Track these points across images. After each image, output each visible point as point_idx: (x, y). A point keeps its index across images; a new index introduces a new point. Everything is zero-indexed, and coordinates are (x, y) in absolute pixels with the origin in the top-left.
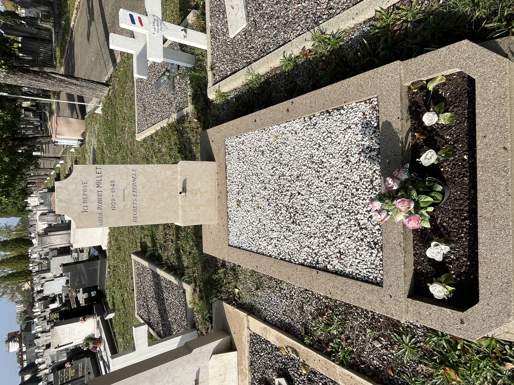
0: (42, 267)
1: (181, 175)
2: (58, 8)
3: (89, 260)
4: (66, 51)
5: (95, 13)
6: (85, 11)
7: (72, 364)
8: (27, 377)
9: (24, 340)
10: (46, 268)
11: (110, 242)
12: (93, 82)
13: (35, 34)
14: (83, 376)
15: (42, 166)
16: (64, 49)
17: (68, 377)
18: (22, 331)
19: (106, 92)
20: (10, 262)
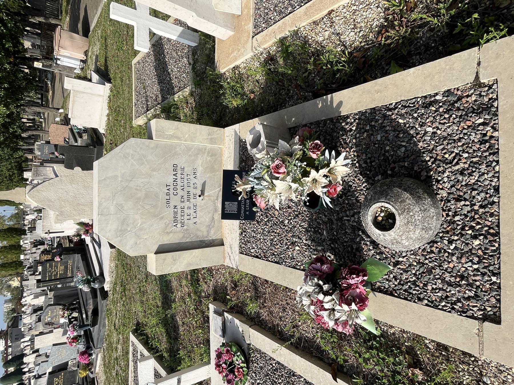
7: (61, 259)
8: (11, 369)
9: (11, 337)
17: (57, 273)
18: (8, 327)
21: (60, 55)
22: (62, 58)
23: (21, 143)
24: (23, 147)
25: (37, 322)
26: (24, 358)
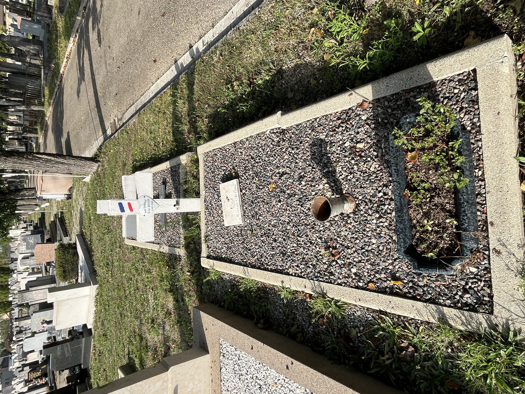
0: (22, 313)
1: (172, 383)
2: (48, 50)
3: (72, 339)
4: (55, 93)
5: (86, 74)
6: (75, 65)
10: (27, 315)
11: (96, 321)
13: (23, 70)
16: (54, 91)
19: (95, 168)
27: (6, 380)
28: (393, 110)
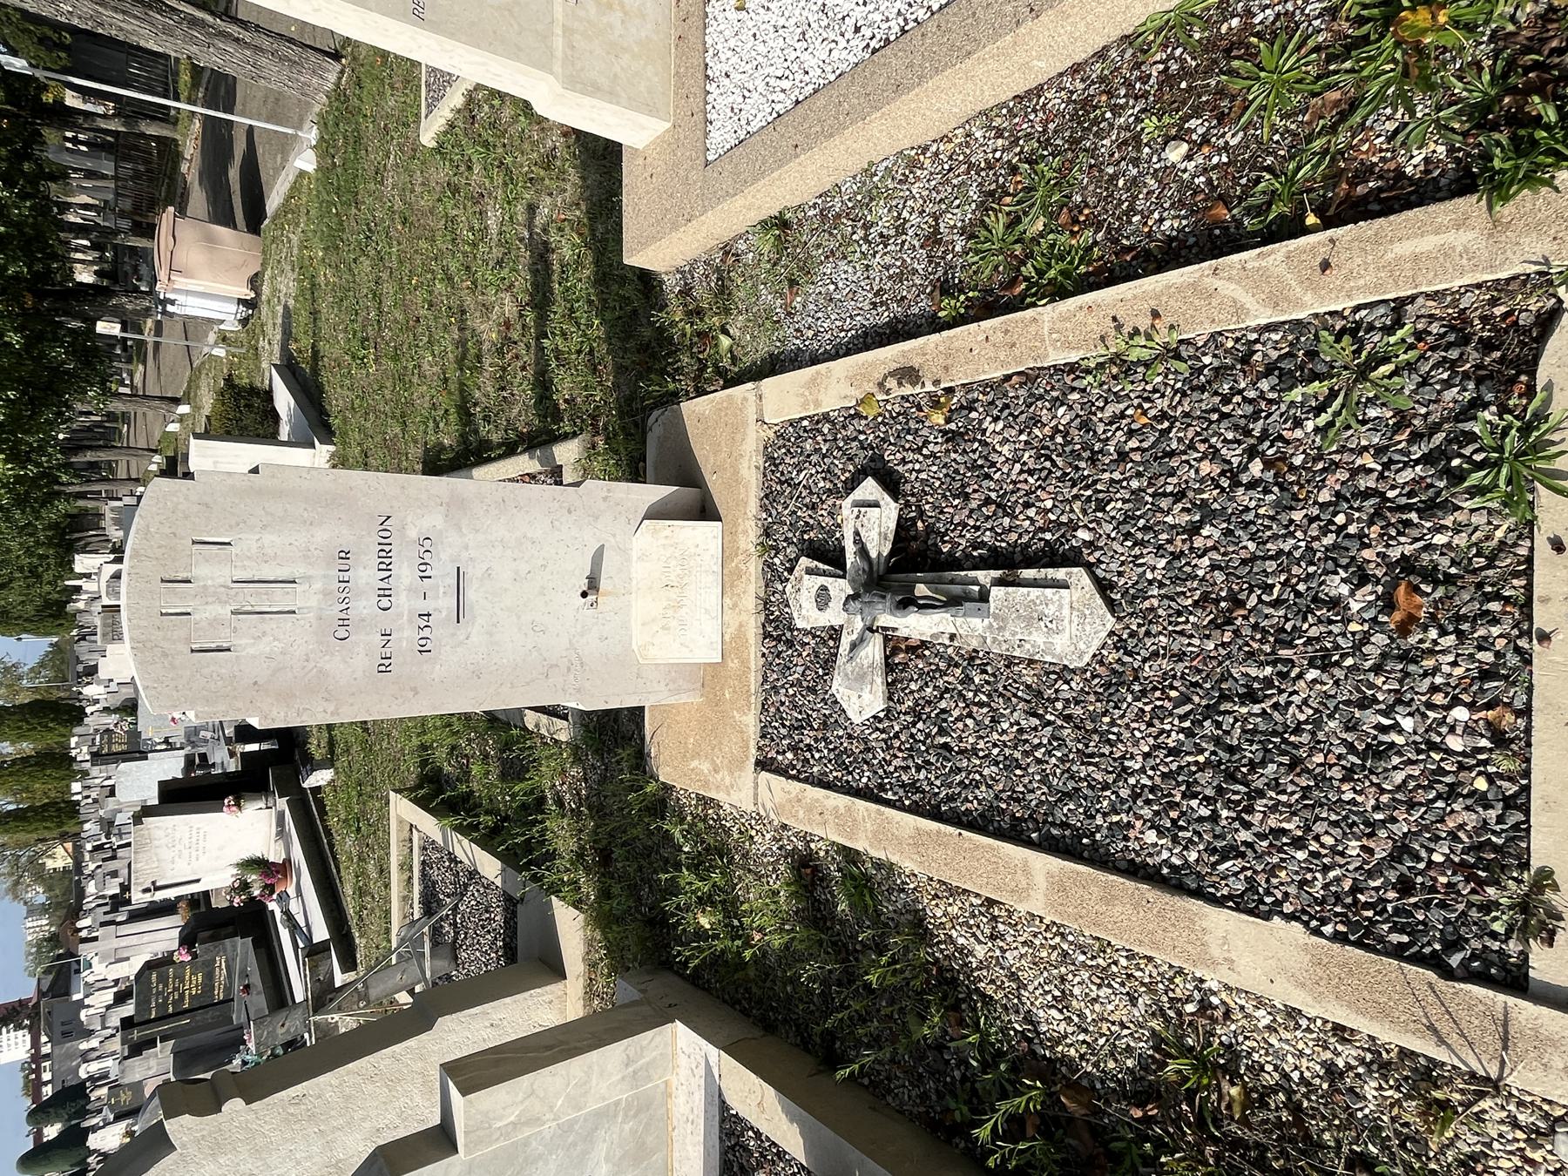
0: (110, 743)
7: (195, 956)
8: (51, 1132)
9: (49, 1025)
10: (124, 747)
12: (291, 40)
14: (228, 1001)
15: (122, 474)
17: (182, 996)
19: (332, 77)
20: (10, 775)
21: (175, 291)
22: (180, 298)
23: (64, 478)
24: (71, 489)
25: (125, 1058)
26: (91, 1137)
27: (63, 1024)
28: (1156, 738)
